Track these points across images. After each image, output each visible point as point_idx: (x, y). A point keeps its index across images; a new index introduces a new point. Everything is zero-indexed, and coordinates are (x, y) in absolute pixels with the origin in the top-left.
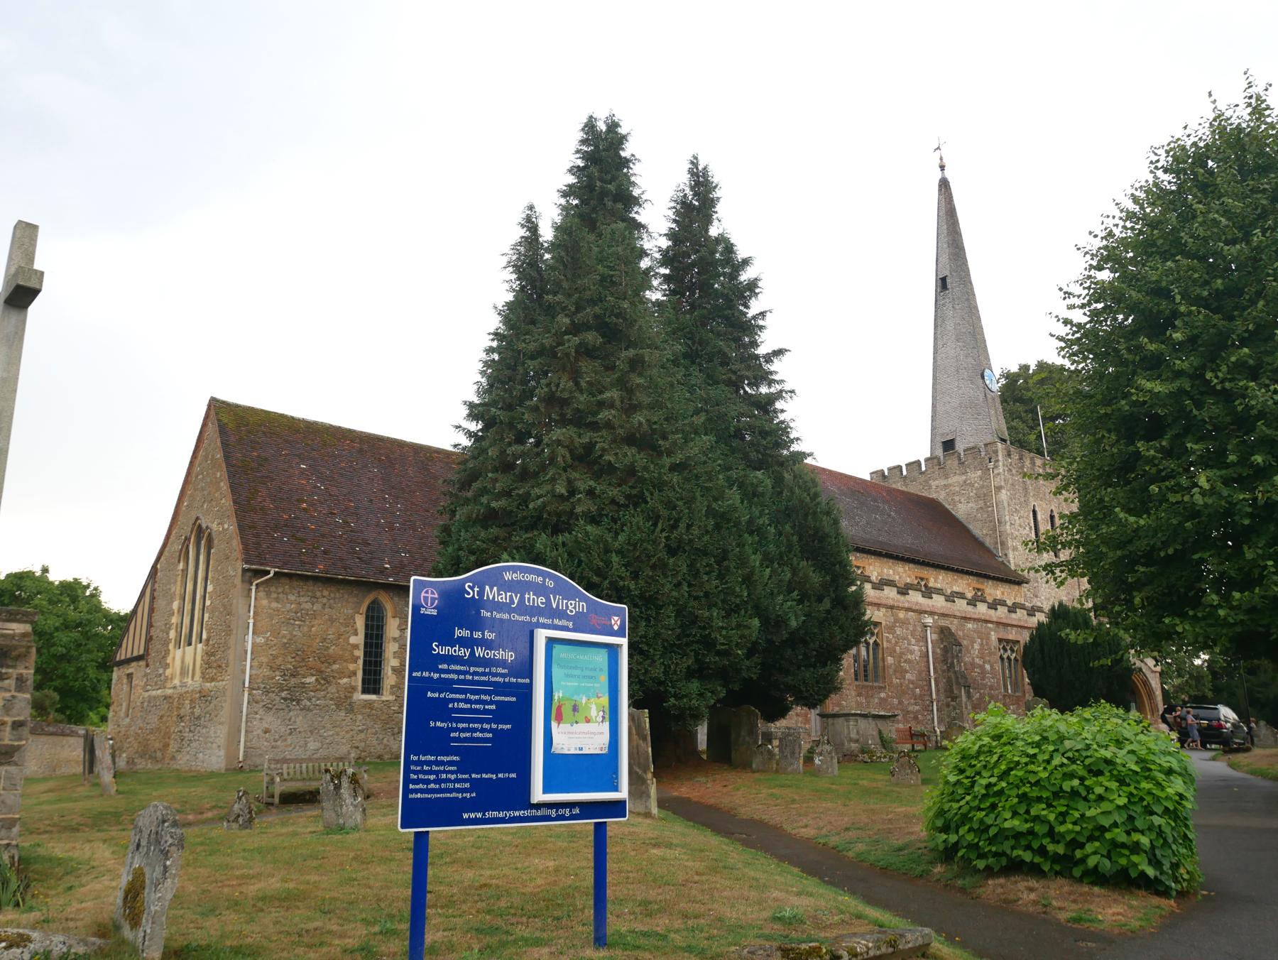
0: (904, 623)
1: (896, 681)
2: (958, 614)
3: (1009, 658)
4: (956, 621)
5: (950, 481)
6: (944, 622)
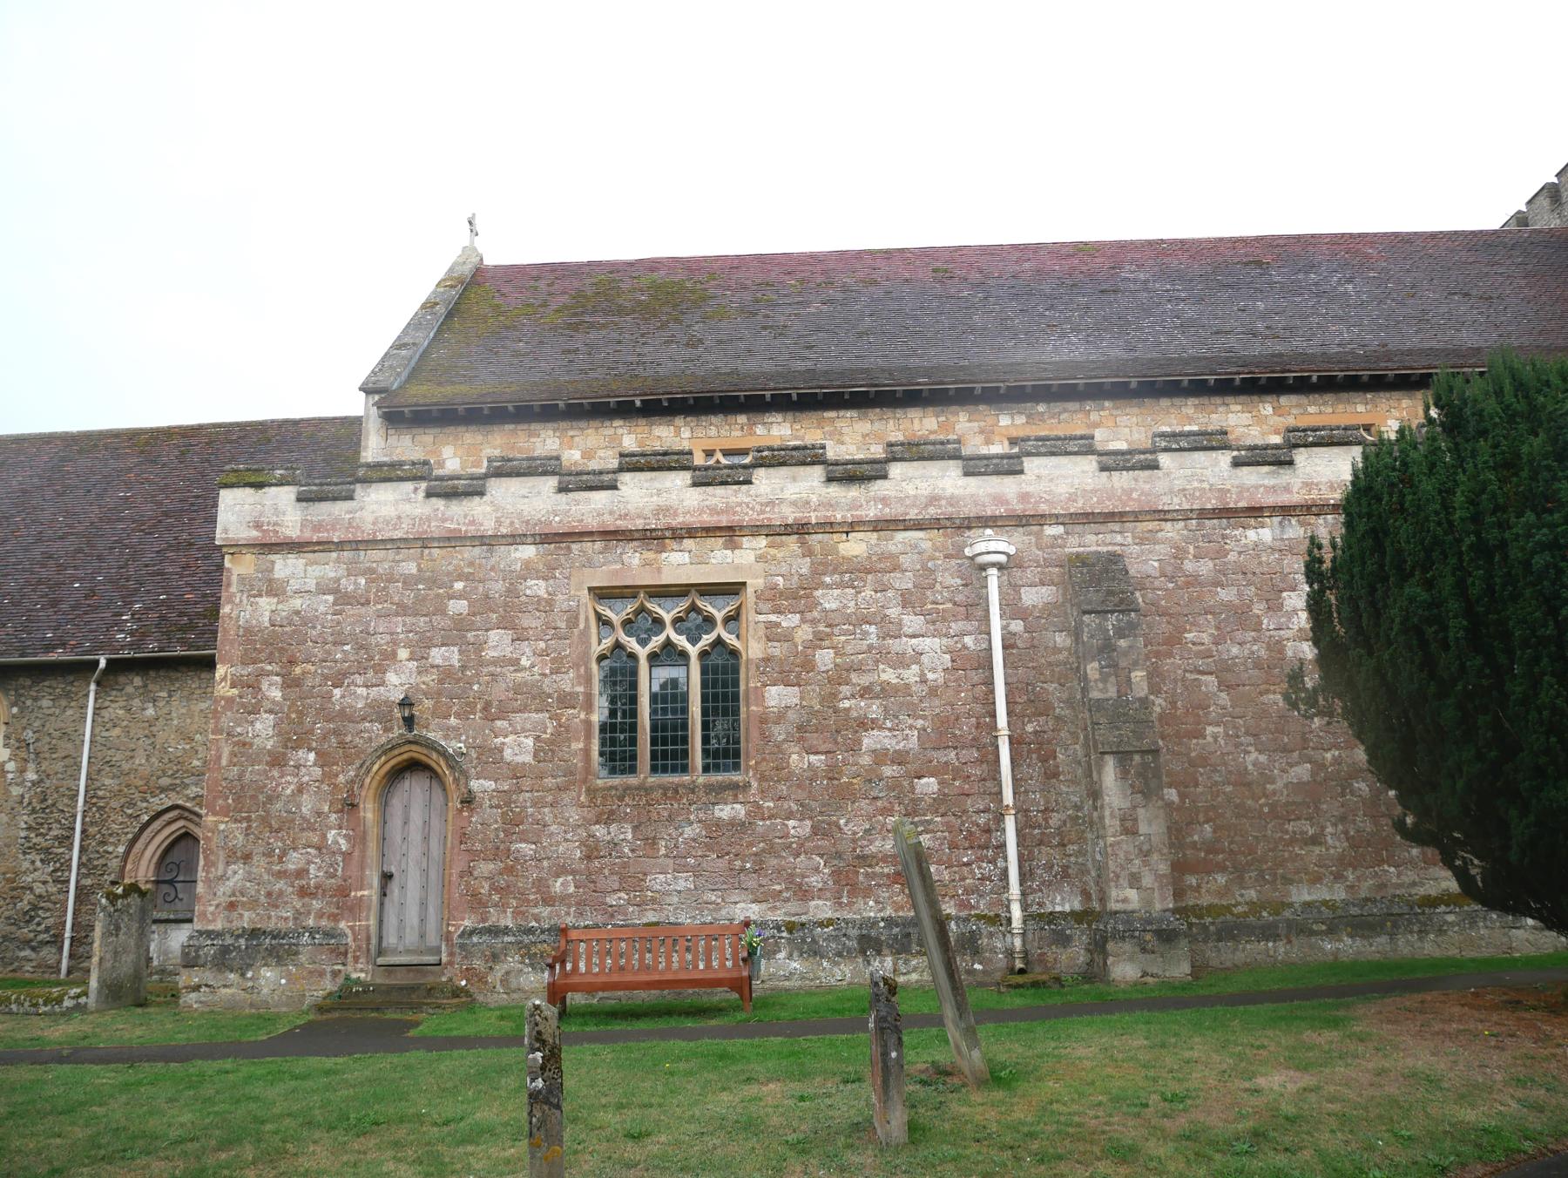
0: (857, 571)
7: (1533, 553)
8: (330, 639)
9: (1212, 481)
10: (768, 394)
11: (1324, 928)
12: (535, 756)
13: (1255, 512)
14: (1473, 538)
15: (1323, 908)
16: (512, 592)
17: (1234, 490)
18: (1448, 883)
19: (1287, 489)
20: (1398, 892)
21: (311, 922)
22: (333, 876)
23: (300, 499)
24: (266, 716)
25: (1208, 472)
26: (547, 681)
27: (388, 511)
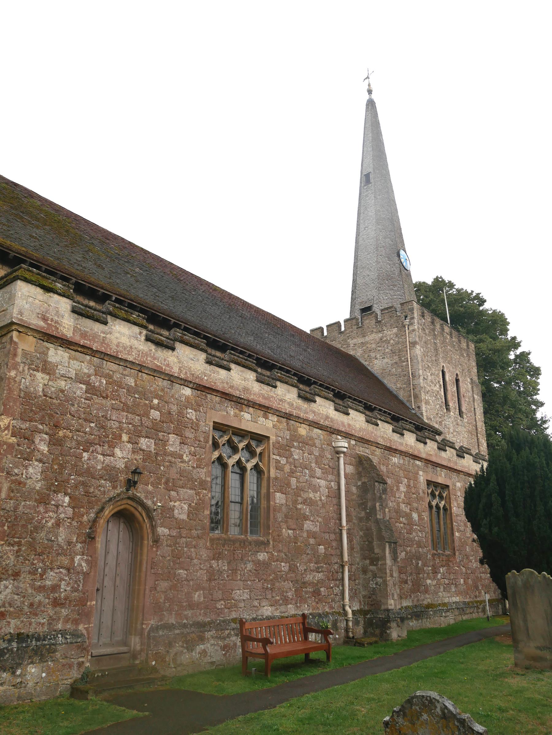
0: (306, 443)
1: (287, 533)
2: (381, 441)
3: (437, 507)
4: (378, 452)
5: (367, 339)
6: (363, 451)
8: (83, 416)
10: (173, 320)
12: (188, 516)
16: (180, 413)
21: (60, 626)
22: (75, 590)
23: (74, 311)
24: (36, 463)
26: (195, 471)
27: (125, 340)
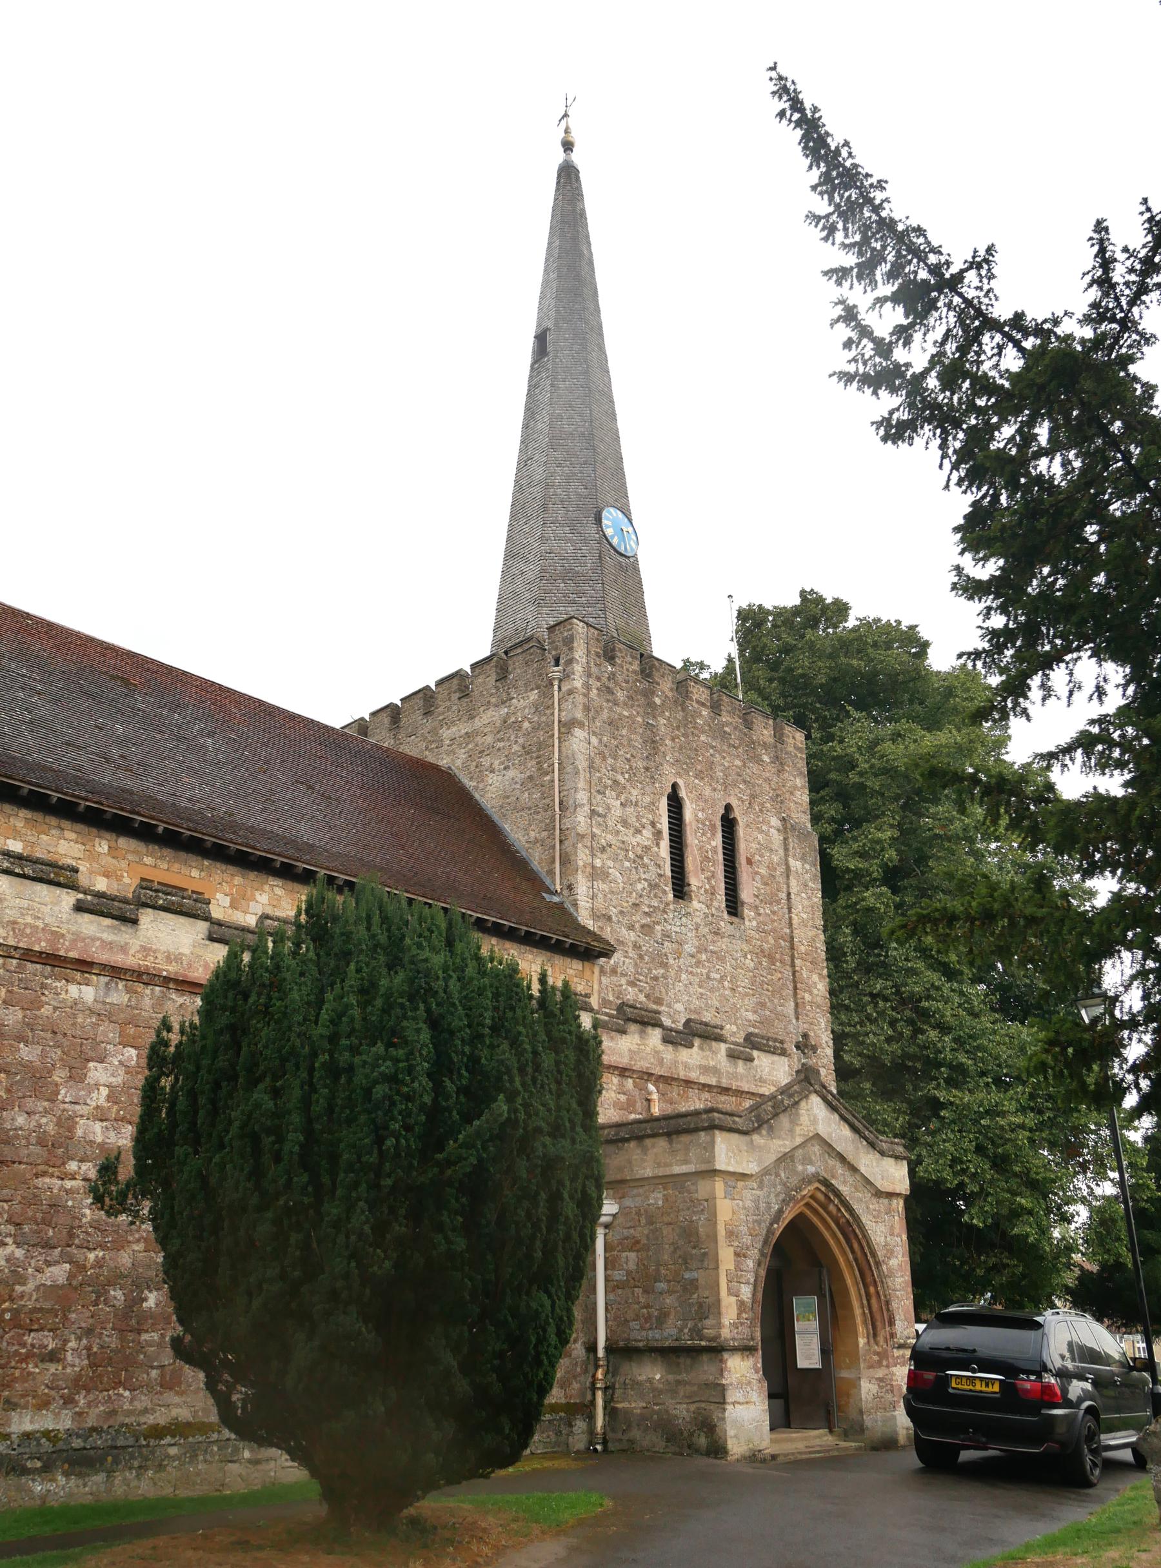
5: (478, 722)
7: (376, 1082)
9: (48, 920)
11: (39, 1464)
13: (84, 966)
14: (327, 1056)
15: (43, 1440)
17: (69, 937)
18: (179, 1410)
19: (124, 949)
20: (127, 1420)
25: (46, 910)
